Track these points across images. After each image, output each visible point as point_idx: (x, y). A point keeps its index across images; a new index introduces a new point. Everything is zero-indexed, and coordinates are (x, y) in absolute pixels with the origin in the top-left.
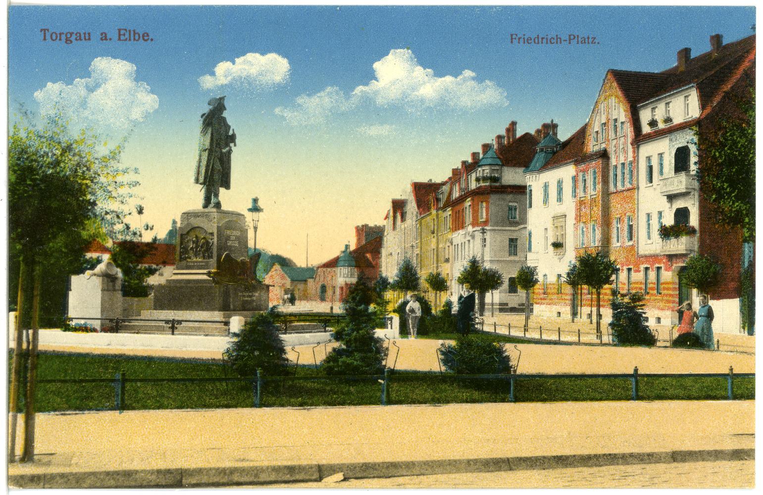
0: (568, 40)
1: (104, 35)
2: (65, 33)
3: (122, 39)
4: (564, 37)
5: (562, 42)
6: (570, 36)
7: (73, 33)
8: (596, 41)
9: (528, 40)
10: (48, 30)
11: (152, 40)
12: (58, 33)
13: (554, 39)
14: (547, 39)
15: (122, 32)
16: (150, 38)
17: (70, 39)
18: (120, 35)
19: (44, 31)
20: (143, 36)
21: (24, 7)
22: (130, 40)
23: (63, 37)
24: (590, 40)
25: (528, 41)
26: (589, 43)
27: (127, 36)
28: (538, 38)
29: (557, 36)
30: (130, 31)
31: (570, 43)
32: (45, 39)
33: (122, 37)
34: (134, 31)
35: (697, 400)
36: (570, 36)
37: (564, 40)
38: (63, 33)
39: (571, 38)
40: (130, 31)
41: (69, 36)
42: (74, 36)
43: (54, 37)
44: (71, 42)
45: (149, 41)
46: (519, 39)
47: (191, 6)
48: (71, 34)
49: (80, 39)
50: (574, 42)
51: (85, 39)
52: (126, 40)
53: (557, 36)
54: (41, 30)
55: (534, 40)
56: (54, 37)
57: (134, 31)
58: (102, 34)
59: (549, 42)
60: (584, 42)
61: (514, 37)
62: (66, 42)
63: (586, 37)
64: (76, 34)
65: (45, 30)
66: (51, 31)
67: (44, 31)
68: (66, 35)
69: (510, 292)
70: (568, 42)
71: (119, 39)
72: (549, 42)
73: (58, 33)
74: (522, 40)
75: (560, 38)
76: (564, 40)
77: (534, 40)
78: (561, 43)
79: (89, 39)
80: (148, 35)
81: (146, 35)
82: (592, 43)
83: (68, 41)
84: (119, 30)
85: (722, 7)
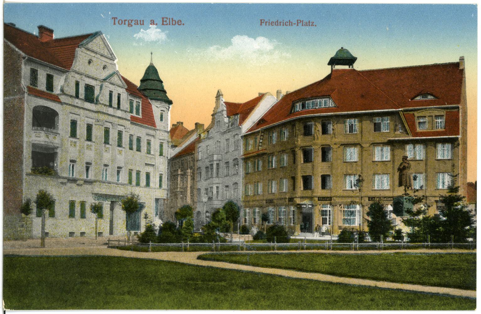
0: (296, 23)
1: (152, 21)
2: (128, 20)
3: (164, 24)
4: (295, 21)
5: (293, 25)
6: (298, 20)
7: (133, 20)
8: (314, 24)
9: (271, 23)
10: (117, 18)
11: (183, 24)
12: (123, 20)
13: (288, 23)
14: (283, 22)
15: (165, 19)
16: (182, 23)
17: (131, 24)
18: (163, 21)
19: (115, 18)
20: (178, 22)
21: (18, 3)
22: (170, 24)
23: (127, 22)
24: (311, 24)
25: (272, 24)
26: (309, 25)
27: (168, 21)
28: (278, 22)
29: (289, 21)
30: (169, 19)
31: (298, 25)
32: (115, 24)
33: (165, 23)
34: (172, 19)
35: (177, 251)
36: (298, 20)
37: (294, 24)
38: (126, 20)
39: (299, 22)
40: (169, 19)
41: (130, 22)
42: (133, 22)
43: (120, 23)
44: (132, 26)
45: (182, 25)
46: (266, 22)
47: (74, 4)
48: (132, 21)
49: (138, 24)
50: (300, 24)
51: (141, 24)
52: (167, 24)
53: (289, 21)
54: (113, 18)
55: (275, 23)
56: (120, 23)
57: (172, 19)
58: (151, 21)
59: (270, 24)
60: (306, 25)
61: (263, 21)
62: (128, 26)
63: (142, 20)
64: (135, 21)
65: (115, 18)
66: (119, 19)
67: (115, 18)
68: (129, 21)
69: (70, 160)
70: (296, 25)
71: (163, 24)
72: (284, 25)
73: (123, 20)
74: (267, 24)
75: (292, 23)
76: (294, 24)
77: (275, 23)
78: (292, 25)
79: (143, 24)
80: (181, 21)
81: (179, 21)
82: (312, 25)
83: (130, 25)
84: (163, 18)
85: (410, 5)
